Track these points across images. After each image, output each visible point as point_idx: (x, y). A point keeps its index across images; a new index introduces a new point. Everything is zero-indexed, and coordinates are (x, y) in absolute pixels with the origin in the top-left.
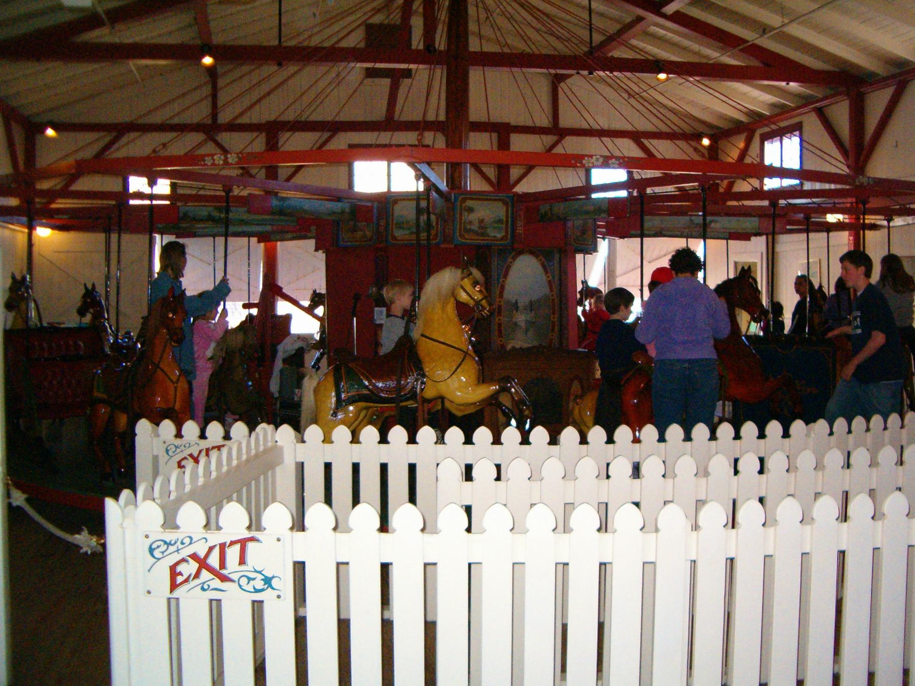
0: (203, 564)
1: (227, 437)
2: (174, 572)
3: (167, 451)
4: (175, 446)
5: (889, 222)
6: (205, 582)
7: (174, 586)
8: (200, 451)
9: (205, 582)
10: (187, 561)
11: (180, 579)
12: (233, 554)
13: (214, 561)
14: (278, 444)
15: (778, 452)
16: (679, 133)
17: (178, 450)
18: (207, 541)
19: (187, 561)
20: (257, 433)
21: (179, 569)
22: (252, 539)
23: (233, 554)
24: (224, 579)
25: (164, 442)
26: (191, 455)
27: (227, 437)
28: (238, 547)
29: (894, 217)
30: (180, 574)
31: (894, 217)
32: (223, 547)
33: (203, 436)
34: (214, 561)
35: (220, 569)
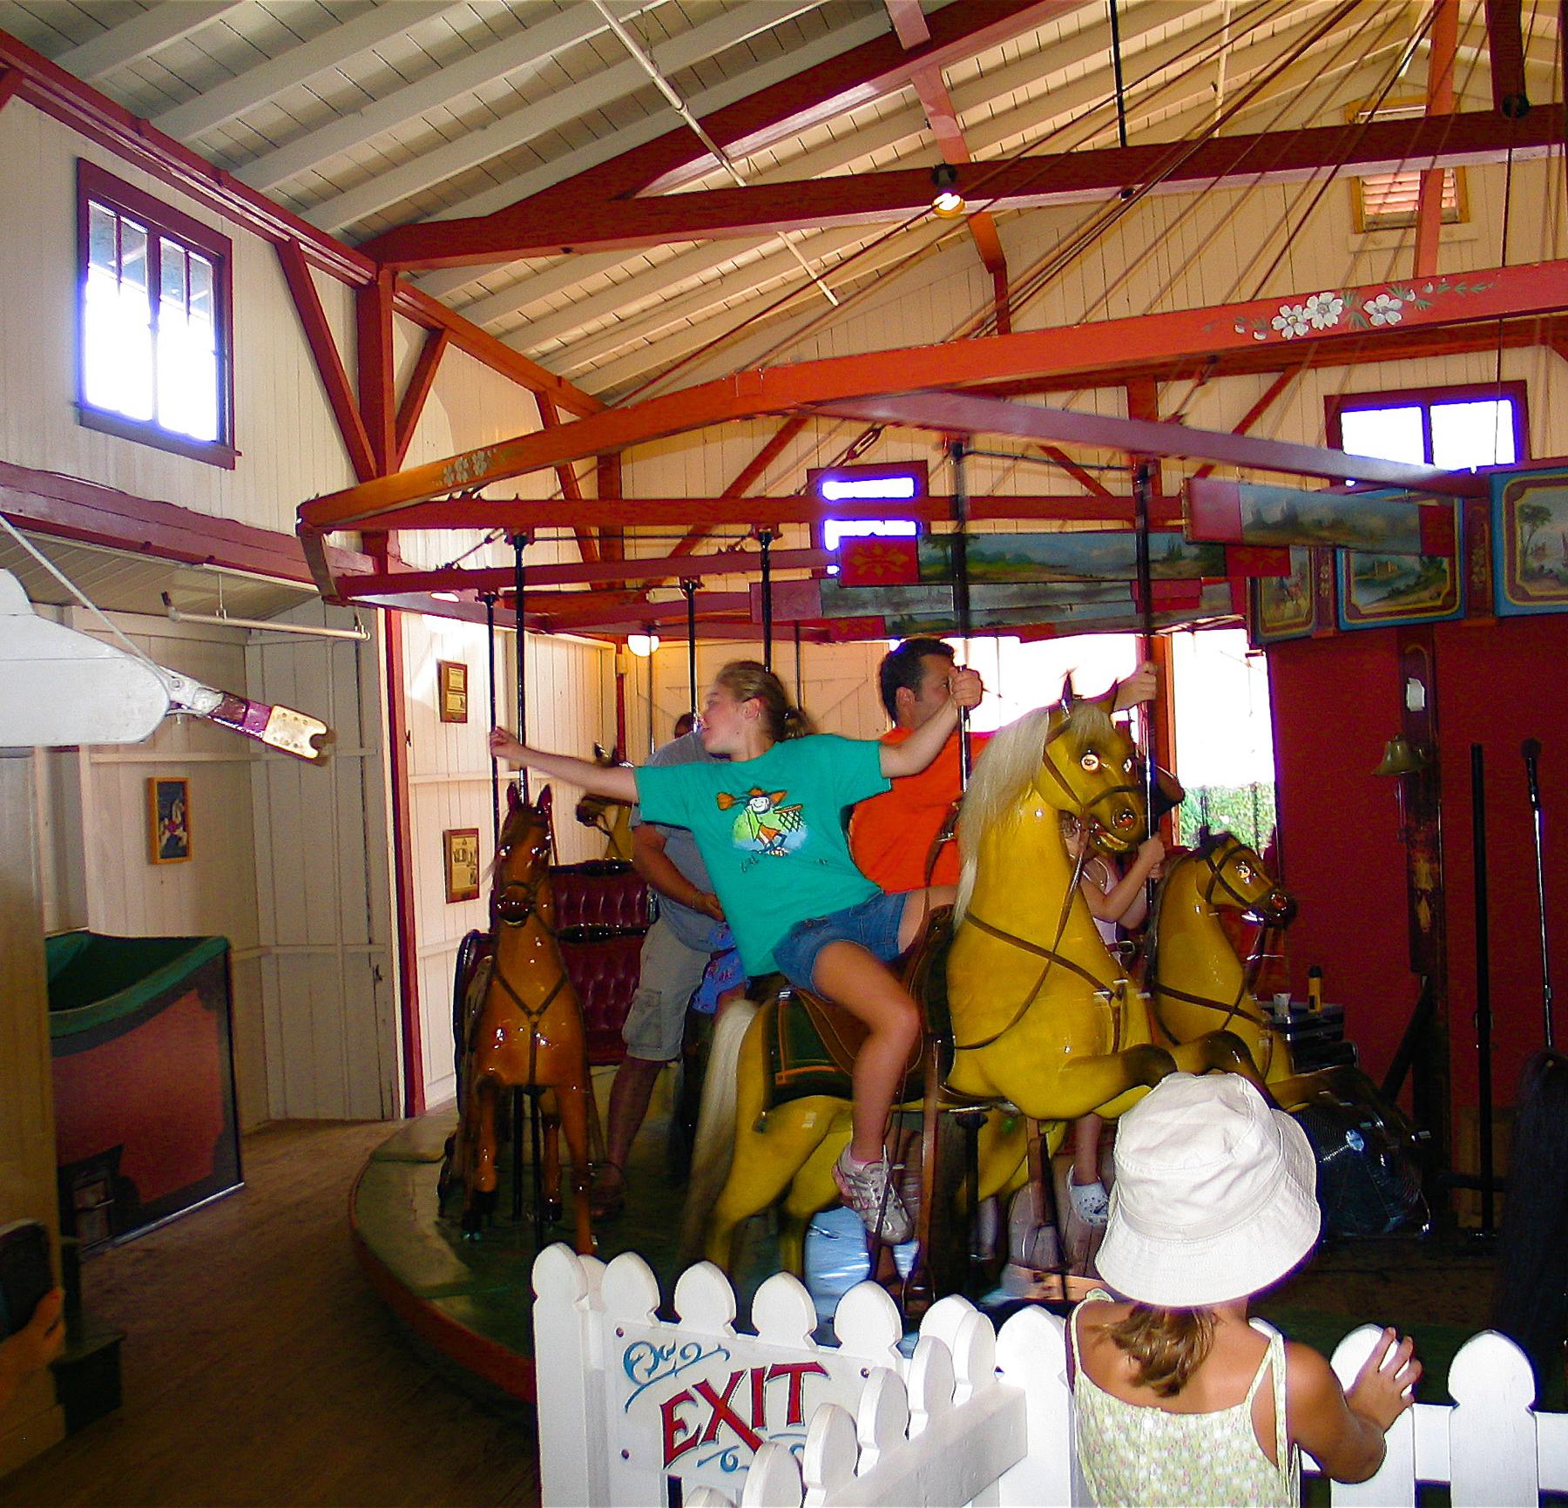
0: (722, 1411)
1: (824, 1334)
2: (671, 1425)
3: (629, 1366)
4: (653, 1349)
5: (765, 539)
6: (729, 1450)
7: (671, 1454)
8: (735, 1378)
9: (729, 1450)
10: (692, 1399)
11: (680, 1438)
12: (777, 1392)
13: (741, 1403)
14: (1003, 1379)
15: (99, 396)
16: (665, 579)
17: (664, 1367)
18: (727, 1358)
19: (692, 1399)
20: (937, 1342)
21: (681, 1412)
22: (815, 1368)
23: (777, 1392)
24: (754, 1443)
25: (620, 1333)
26: (704, 1388)
27: (824, 1334)
28: (784, 1382)
29: (782, 527)
30: (682, 1425)
31: (782, 527)
32: (758, 1377)
33: (743, 1323)
34: (741, 1403)
35: (753, 1427)
